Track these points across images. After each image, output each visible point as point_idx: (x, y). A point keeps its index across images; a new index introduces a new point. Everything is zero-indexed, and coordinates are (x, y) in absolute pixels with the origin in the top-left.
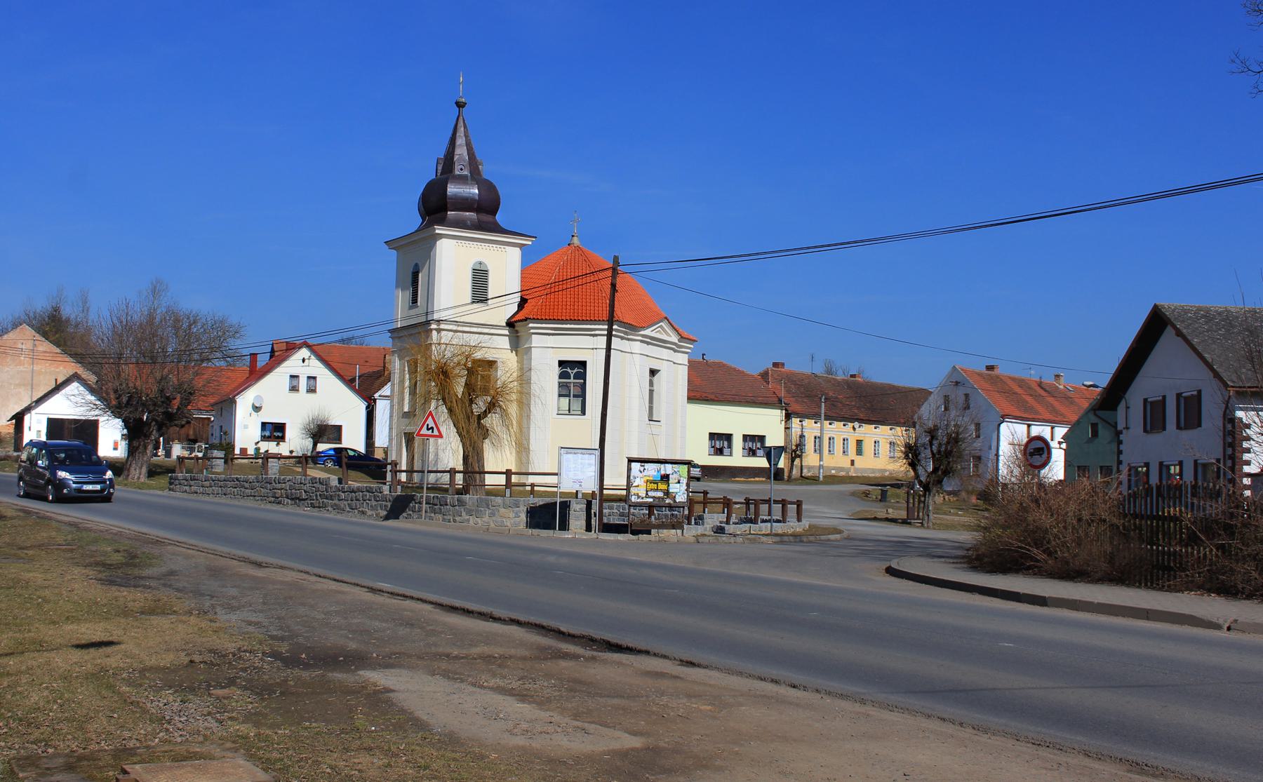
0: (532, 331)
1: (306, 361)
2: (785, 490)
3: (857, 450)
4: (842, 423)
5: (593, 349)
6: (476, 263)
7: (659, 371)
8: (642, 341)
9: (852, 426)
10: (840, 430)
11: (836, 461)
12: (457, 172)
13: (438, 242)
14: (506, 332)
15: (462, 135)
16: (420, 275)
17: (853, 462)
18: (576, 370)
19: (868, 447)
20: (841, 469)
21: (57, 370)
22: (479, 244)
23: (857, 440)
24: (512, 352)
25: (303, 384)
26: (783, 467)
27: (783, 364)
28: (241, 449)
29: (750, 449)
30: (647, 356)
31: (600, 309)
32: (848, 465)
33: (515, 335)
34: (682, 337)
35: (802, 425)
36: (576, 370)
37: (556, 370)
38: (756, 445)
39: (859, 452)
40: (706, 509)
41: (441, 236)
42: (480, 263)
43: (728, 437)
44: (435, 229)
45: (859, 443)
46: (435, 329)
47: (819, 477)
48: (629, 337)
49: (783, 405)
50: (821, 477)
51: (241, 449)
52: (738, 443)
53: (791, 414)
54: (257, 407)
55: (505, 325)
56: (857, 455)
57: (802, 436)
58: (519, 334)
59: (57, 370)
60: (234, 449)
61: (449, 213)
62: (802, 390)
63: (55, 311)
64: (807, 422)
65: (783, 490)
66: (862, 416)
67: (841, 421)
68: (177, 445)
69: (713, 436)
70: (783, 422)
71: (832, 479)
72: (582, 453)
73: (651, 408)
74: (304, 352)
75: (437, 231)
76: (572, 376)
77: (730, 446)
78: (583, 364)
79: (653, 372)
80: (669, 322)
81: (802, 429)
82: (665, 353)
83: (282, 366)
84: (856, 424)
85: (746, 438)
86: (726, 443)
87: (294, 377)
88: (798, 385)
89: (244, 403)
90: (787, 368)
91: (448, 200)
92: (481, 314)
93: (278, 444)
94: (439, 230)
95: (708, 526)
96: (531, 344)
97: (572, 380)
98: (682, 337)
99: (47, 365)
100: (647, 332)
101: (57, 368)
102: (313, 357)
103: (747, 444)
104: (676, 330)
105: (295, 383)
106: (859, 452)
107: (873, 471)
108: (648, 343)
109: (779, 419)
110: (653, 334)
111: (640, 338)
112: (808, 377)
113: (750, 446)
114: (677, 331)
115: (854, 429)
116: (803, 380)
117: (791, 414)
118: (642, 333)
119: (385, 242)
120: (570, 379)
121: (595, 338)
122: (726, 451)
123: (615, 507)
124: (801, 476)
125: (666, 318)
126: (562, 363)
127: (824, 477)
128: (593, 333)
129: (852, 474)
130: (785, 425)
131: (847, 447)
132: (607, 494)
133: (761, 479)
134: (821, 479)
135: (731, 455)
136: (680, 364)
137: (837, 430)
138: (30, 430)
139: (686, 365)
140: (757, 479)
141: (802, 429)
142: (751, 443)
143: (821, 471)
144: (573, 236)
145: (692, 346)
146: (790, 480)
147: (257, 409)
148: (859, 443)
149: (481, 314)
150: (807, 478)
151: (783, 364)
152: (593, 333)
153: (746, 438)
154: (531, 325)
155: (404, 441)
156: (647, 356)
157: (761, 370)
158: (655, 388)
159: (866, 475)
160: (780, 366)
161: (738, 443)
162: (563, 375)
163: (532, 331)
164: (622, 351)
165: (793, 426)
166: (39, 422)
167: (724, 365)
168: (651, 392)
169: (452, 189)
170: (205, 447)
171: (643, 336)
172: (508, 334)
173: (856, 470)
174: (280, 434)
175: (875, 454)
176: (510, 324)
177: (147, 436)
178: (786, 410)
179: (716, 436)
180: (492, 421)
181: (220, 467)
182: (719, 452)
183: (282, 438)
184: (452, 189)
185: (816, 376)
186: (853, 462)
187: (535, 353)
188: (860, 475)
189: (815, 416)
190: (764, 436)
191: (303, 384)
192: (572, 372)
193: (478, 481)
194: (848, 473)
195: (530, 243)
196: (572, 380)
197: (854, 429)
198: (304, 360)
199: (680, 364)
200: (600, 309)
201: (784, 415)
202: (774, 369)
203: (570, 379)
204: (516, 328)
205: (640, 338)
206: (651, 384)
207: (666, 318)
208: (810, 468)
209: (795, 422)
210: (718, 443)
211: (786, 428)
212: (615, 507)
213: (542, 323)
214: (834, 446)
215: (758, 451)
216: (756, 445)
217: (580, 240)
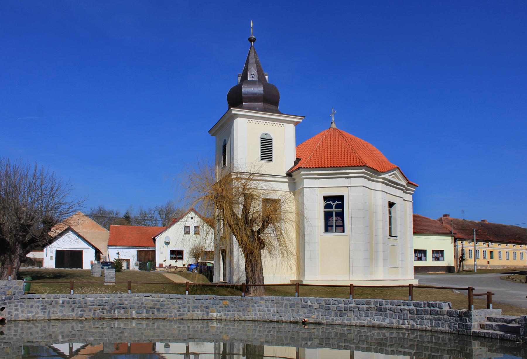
0: (304, 177)
3: (490, 256)
4: (483, 243)
5: (348, 187)
7: (395, 203)
8: (383, 183)
9: (487, 244)
10: (481, 246)
11: (481, 262)
12: (249, 79)
13: (235, 121)
14: (286, 180)
16: (227, 147)
17: (488, 262)
18: (336, 203)
19: (496, 255)
20: (483, 266)
21: (95, 231)
23: (490, 251)
24: (290, 193)
25: (192, 230)
27: (449, 215)
28: (159, 264)
29: (436, 257)
30: (387, 193)
32: (486, 263)
33: (293, 182)
34: (409, 183)
35: (462, 244)
36: (336, 203)
38: (435, 255)
39: (491, 257)
40: (473, 306)
41: (237, 116)
42: (266, 134)
43: (424, 252)
44: (231, 111)
45: (491, 252)
46: (235, 179)
47: (474, 270)
49: (453, 234)
51: (159, 264)
52: (429, 254)
54: (167, 243)
55: (285, 175)
56: (491, 258)
57: (463, 250)
58: (295, 181)
59: (95, 231)
60: (155, 265)
61: (244, 103)
63: (127, 213)
64: (465, 243)
66: (492, 239)
67: (482, 242)
68: (125, 263)
70: (453, 243)
71: (481, 271)
72: (214, 128)
74: (192, 214)
75: (233, 112)
76: (334, 206)
77: (425, 256)
79: (391, 205)
80: (400, 171)
81: (462, 246)
82: (399, 193)
84: (490, 243)
86: (423, 255)
87: (187, 227)
89: (160, 240)
90: (451, 217)
91: (243, 95)
92: (267, 167)
93: (176, 261)
98: (409, 183)
99: (90, 229)
100: (386, 176)
101: (95, 230)
102: (196, 216)
103: (434, 255)
104: (404, 177)
105: (188, 230)
106: (491, 257)
107: (499, 266)
108: (387, 184)
109: (450, 241)
110: (390, 178)
111: (381, 180)
112: (462, 221)
115: (488, 245)
116: (459, 223)
117: (457, 239)
118: (382, 176)
119: (208, 132)
120: (332, 208)
122: (423, 258)
123: (372, 303)
124: (463, 270)
125: (398, 168)
126: (326, 198)
127: (477, 270)
128: (347, 175)
129: (489, 268)
131: (486, 255)
132: (248, 93)
133: (443, 272)
134: (476, 271)
135: (426, 260)
136: (408, 201)
137: (481, 246)
138: (47, 256)
139: (411, 202)
140: (441, 272)
143: (476, 267)
144: (332, 123)
148: (491, 252)
149: (267, 167)
150: (466, 271)
151: (449, 215)
152: (347, 175)
153: (434, 251)
154: (302, 172)
155: (221, 253)
156: (387, 193)
158: (392, 215)
159: (495, 268)
160: (447, 216)
161: (429, 254)
162: (327, 206)
163: (304, 177)
164: (369, 189)
165: (458, 245)
166: (52, 252)
168: (390, 217)
169: (245, 90)
171: (384, 179)
172: (288, 181)
173: (490, 266)
174: (181, 257)
175: (499, 258)
176: (289, 174)
177: (13, 252)
178: (454, 237)
179: (422, 251)
180: (269, 235)
181: (98, 274)
182: (420, 259)
183: (182, 259)
184: (245, 90)
185: (466, 221)
186: (488, 262)
188: (492, 268)
189: (471, 240)
190: (443, 250)
191: (192, 230)
192: (334, 204)
193: (257, 281)
194: (486, 267)
197: (488, 245)
199: (408, 201)
201: (453, 239)
202: (444, 217)
203: (332, 208)
204: (293, 177)
205: (381, 180)
206: (390, 212)
207: (398, 168)
208: (467, 266)
209: (459, 242)
210: (419, 255)
211: (455, 246)
212: (372, 303)
214: (479, 255)
215: (441, 258)
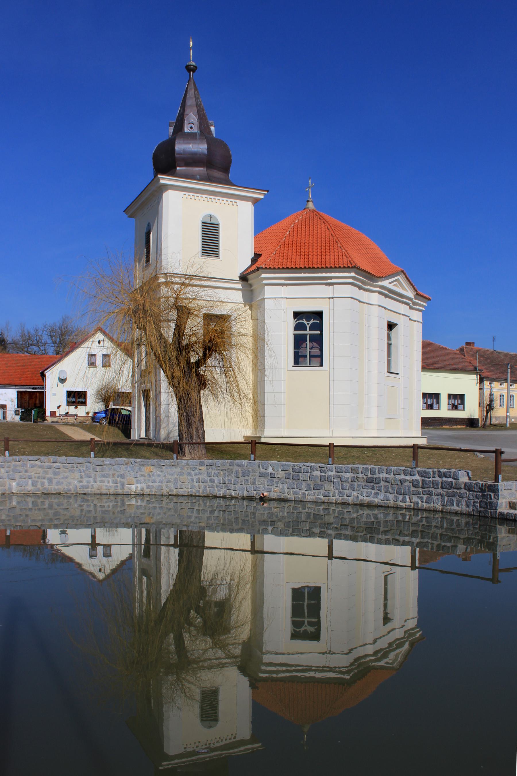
0: (265, 282)
1: (102, 342)
2: (488, 435)
5: (329, 298)
6: (207, 215)
8: (380, 293)
12: (186, 130)
13: (164, 194)
14: (239, 286)
15: (193, 96)
16: (151, 235)
18: (312, 321)
22: (209, 197)
24: (245, 306)
25: (99, 360)
26: (477, 417)
27: (473, 343)
28: (51, 412)
30: (385, 308)
31: (336, 257)
35: (491, 387)
36: (312, 321)
37: (291, 322)
38: (458, 402)
40: (500, 477)
41: (166, 187)
42: (210, 217)
43: (437, 396)
44: (159, 179)
46: (163, 283)
47: (506, 424)
48: (366, 287)
49: (478, 371)
50: (508, 424)
51: (51, 412)
52: (444, 400)
53: (484, 378)
54: (62, 380)
55: (238, 279)
57: (491, 395)
58: (252, 288)
61: (178, 168)
62: (489, 361)
65: (486, 435)
69: (425, 395)
70: (478, 385)
73: (389, 362)
74: (99, 336)
75: (162, 181)
76: (308, 327)
77: (438, 403)
78: (319, 315)
79: (391, 326)
80: (406, 276)
82: (403, 308)
83: (82, 346)
85: (450, 396)
86: (435, 400)
88: (485, 358)
90: (476, 346)
93: (76, 408)
94: (164, 180)
95: (504, 501)
96: (264, 295)
97: (308, 332)
98: (417, 294)
100: (385, 283)
102: (106, 339)
103: (450, 401)
105: (93, 360)
108: (386, 296)
109: (475, 382)
110: (391, 287)
111: (378, 289)
112: (491, 353)
113: (453, 402)
114: (413, 286)
116: (488, 354)
117: (484, 378)
118: (380, 283)
121: (331, 287)
122: (435, 406)
123: (360, 470)
124: (491, 424)
125: (403, 272)
126: (297, 315)
127: (510, 424)
128: (329, 281)
130: (480, 386)
132: (185, 152)
133: (462, 427)
134: (508, 425)
135: (439, 409)
136: (415, 321)
140: (459, 427)
141: (491, 389)
142: (453, 401)
143: (508, 420)
144: (308, 201)
145: (425, 304)
146: (484, 427)
147: (63, 381)
150: (495, 425)
151: (473, 343)
152: (329, 281)
154: (263, 275)
156: (385, 308)
157: (459, 347)
158: (393, 341)
160: (471, 345)
161: (444, 400)
162: (298, 327)
163: (265, 282)
164: (360, 301)
165: (485, 387)
167: (431, 344)
168: (389, 345)
169: (180, 147)
170: (22, 411)
171: (382, 287)
176: (244, 278)
178: (480, 376)
179: (427, 395)
182: (430, 407)
183: (84, 403)
185: (497, 352)
187: (268, 304)
189: (503, 380)
191: (99, 360)
192: (308, 323)
193: (195, 437)
195: (262, 197)
196: (308, 332)
198: (99, 342)
199: (415, 321)
200: (336, 257)
201: (478, 379)
202: (467, 346)
204: (250, 282)
205: (378, 289)
208: (497, 418)
210: (429, 400)
212: (360, 470)
213: (275, 273)
215: (459, 406)
216: (458, 402)
217: (315, 205)
